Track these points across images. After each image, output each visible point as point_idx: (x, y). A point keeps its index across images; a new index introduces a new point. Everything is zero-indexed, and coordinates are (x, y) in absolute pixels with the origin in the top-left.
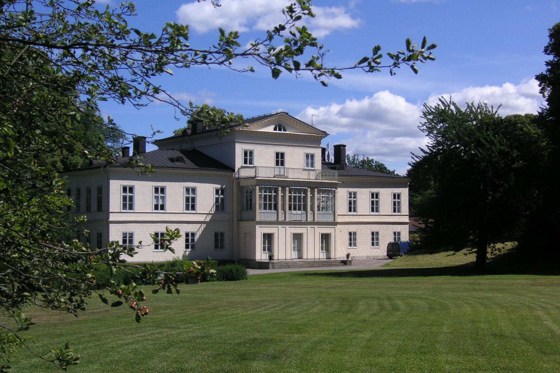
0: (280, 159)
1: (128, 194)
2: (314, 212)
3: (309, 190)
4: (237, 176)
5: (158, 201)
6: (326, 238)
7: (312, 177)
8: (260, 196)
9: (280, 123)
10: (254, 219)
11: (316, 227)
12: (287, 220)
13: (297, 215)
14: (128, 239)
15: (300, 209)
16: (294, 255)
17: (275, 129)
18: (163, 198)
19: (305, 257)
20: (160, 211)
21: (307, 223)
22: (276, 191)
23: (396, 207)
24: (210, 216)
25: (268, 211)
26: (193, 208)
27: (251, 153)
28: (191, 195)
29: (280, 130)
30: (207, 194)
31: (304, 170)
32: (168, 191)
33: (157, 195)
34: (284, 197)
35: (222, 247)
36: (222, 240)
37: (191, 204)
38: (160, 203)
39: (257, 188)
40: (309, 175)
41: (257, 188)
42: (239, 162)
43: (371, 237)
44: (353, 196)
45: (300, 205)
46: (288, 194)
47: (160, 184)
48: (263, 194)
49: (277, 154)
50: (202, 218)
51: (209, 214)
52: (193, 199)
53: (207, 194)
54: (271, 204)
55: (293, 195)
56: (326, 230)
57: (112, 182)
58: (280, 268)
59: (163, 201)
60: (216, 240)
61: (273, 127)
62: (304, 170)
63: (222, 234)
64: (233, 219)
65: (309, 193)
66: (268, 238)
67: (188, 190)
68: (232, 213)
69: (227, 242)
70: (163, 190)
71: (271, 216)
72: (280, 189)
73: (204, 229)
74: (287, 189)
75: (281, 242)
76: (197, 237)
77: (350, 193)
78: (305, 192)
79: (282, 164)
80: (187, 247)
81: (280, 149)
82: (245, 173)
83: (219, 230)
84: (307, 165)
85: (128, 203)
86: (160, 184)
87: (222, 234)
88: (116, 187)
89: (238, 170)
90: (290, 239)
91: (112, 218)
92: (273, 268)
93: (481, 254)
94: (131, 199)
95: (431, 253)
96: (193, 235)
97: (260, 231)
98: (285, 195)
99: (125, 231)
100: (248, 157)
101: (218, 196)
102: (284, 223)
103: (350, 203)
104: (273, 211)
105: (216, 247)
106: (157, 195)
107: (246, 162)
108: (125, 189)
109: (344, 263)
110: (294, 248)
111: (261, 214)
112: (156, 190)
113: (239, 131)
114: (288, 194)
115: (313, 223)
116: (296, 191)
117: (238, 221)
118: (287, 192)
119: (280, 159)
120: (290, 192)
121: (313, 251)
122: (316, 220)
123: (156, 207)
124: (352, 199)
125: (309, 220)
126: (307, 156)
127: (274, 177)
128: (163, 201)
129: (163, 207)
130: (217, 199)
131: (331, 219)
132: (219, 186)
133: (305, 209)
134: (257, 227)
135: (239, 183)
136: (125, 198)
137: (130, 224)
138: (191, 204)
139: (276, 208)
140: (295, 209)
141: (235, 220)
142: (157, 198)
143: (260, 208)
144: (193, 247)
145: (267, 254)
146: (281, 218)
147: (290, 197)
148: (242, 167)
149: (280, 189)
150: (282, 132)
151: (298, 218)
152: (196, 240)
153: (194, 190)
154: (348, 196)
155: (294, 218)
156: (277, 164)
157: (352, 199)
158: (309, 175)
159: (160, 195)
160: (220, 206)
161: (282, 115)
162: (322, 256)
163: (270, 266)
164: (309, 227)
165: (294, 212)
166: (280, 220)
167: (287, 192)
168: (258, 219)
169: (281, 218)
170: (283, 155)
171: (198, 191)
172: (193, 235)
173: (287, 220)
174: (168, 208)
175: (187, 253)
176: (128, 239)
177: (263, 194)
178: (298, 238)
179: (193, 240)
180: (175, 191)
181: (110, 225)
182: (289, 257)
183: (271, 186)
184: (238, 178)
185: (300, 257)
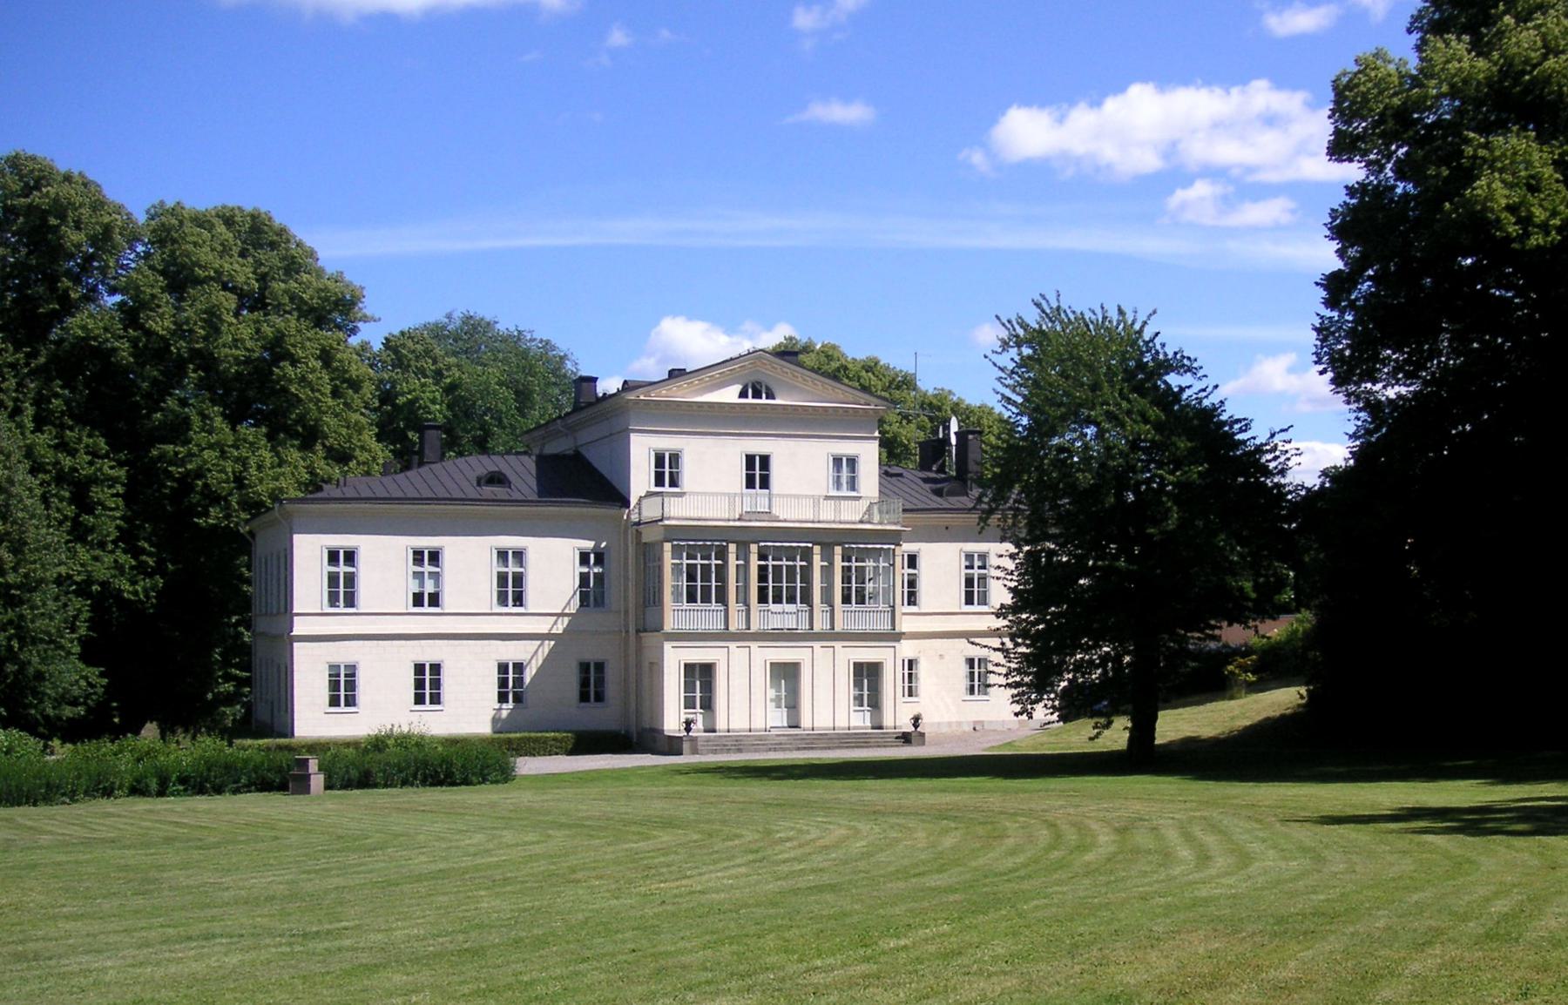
0: (758, 472)
1: (342, 569)
2: (747, 604)
3: (817, 549)
4: (635, 518)
5: (422, 584)
6: (867, 674)
7: (849, 514)
8: (676, 569)
9: (753, 378)
10: (659, 628)
11: (838, 645)
12: (754, 628)
13: (784, 615)
14: (342, 679)
15: (791, 600)
16: (778, 718)
17: (743, 394)
18: (436, 577)
19: (806, 722)
20: (426, 609)
21: (811, 636)
22: (722, 554)
23: (973, 591)
24: (566, 620)
25: (699, 605)
26: (519, 600)
27: (675, 458)
28: (512, 568)
29: (757, 395)
30: (555, 565)
31: (827, 498)
32: (447, 558)
33: (419, 569)
34: (828, 572)
35: (600, 697)
36: (600, 682)
37: (512, 590)
38: (429, 587)
39: (667, 546)
40: (838, 511)
41: (667, 546)
42: (640, 480)
43: (965, 669)
44: (977, 563)
45: (792, 591)
46: (839, 563)
47: (426, 542)
48: (686, 562)
49: (750, 459)
50: (543, 626)
51: (562, 615)
52: (519, 580)
53: (555, 565)
54: (704, 587)
55: (771, 563)
56: (867, 654)
57: (299, 539)
58: (715, 752)
59: (437, 584)
60: (584, 683)
61: (738, 388)
62: (827, 498)
63: (600, 667)
64: (626, 626)
65: (817, 559)
66: (701, 677)
67: (502, 555)
68: (626, 612)
69: (612, 689)
70: (435, 557)
71: (706, 617)
72: (732, 548)
73: (551, 651)
74: (838, 550)
75: (744, 684)
76: (528, 676)
77: (969, 557)
78: (807, 555)
79: (765, 484)
80: (503, 698)
81: (758, 446)
82: (650, 511)
83: (591, 656)
84: (838, 485)
85: (343, 591)
86: (426, 542)
87: (600, 667)
88: (309, 553)
89: (639, 503)
90: (761, 676)
91: (300, 627)
92: (695, 751)
93: (1143, 730)
94: (351, 580)
95: (1268, 719)
96: (519, 667)
97: (674, 659)
98: (746, 566)
99: (335, 660)
100: (667, 470)
101: (585, 570)
102: (745, 636)
103: (969, 582)
104: (714, 605)
105: (584, 697)
106: (419, 569)
107: (659, 481)
108: (333, 557)
109: (906, 738)
110: (777, 700)
111: (676, 614)
112: (418, 556)
113: (638, 402)
114: (839, 563)
115: (831, 636)
116: (779, 553)
117: (638, 631)
118: (838, 559)
119: (758, 472)
120: (762, 557)
121: (830, 706)
122: (837, 629)
123: (418, 600)
124: (976, 572)
125: (817, 628)
126: (837, 461)
127: (861, 522)
128: (437, 584)
129: (435, 600)
130: (584, 579)
131: (884, 626)
132: (589, 545)
133: (807, 599)
134: (667, 646)
135: (639, 533)
136: (333, 579)
137: (423, 642)
138: (512, 590)
139: (722, 598)
140: (777, 600)
141: (632, 630)
142: (418, 576)
143: (677, 599)
144: (518, 699)
145: (868, 715)
146: (736, 624)
147: (763, 570)
148: (650, 494)
149: (732, 548)
150: (764, 401)
151: (790, 623)
152: (527, 680)
153: (519, 555)
154: (964, 563)
155: (776, 623)
156: (750, 484)
157: (976, 572)
158: (838, 511)
159: (427, 568)
160: (591, 594)
161: (760, 358)
162: (860, 720)
163: (686, 746)
164: (817, 645)
165: (773, 607)
166: (732, 628)
167: (838, 559)
168: (669, 625)
169: (736, 624)
170: (765, 461)
171: (531, 558)
172: (519, 667)
173: (754, 628)
174: (449, 602)
175: (504, 714)
176: (342, 679)
177: (686, 562)
178: (786, 674)
179: (519, 681)
180: (469, 560)
181: (296, 645)
182: (758, 724)
183: (707, 546)
184: (639, 524)
185: (795, 725)
